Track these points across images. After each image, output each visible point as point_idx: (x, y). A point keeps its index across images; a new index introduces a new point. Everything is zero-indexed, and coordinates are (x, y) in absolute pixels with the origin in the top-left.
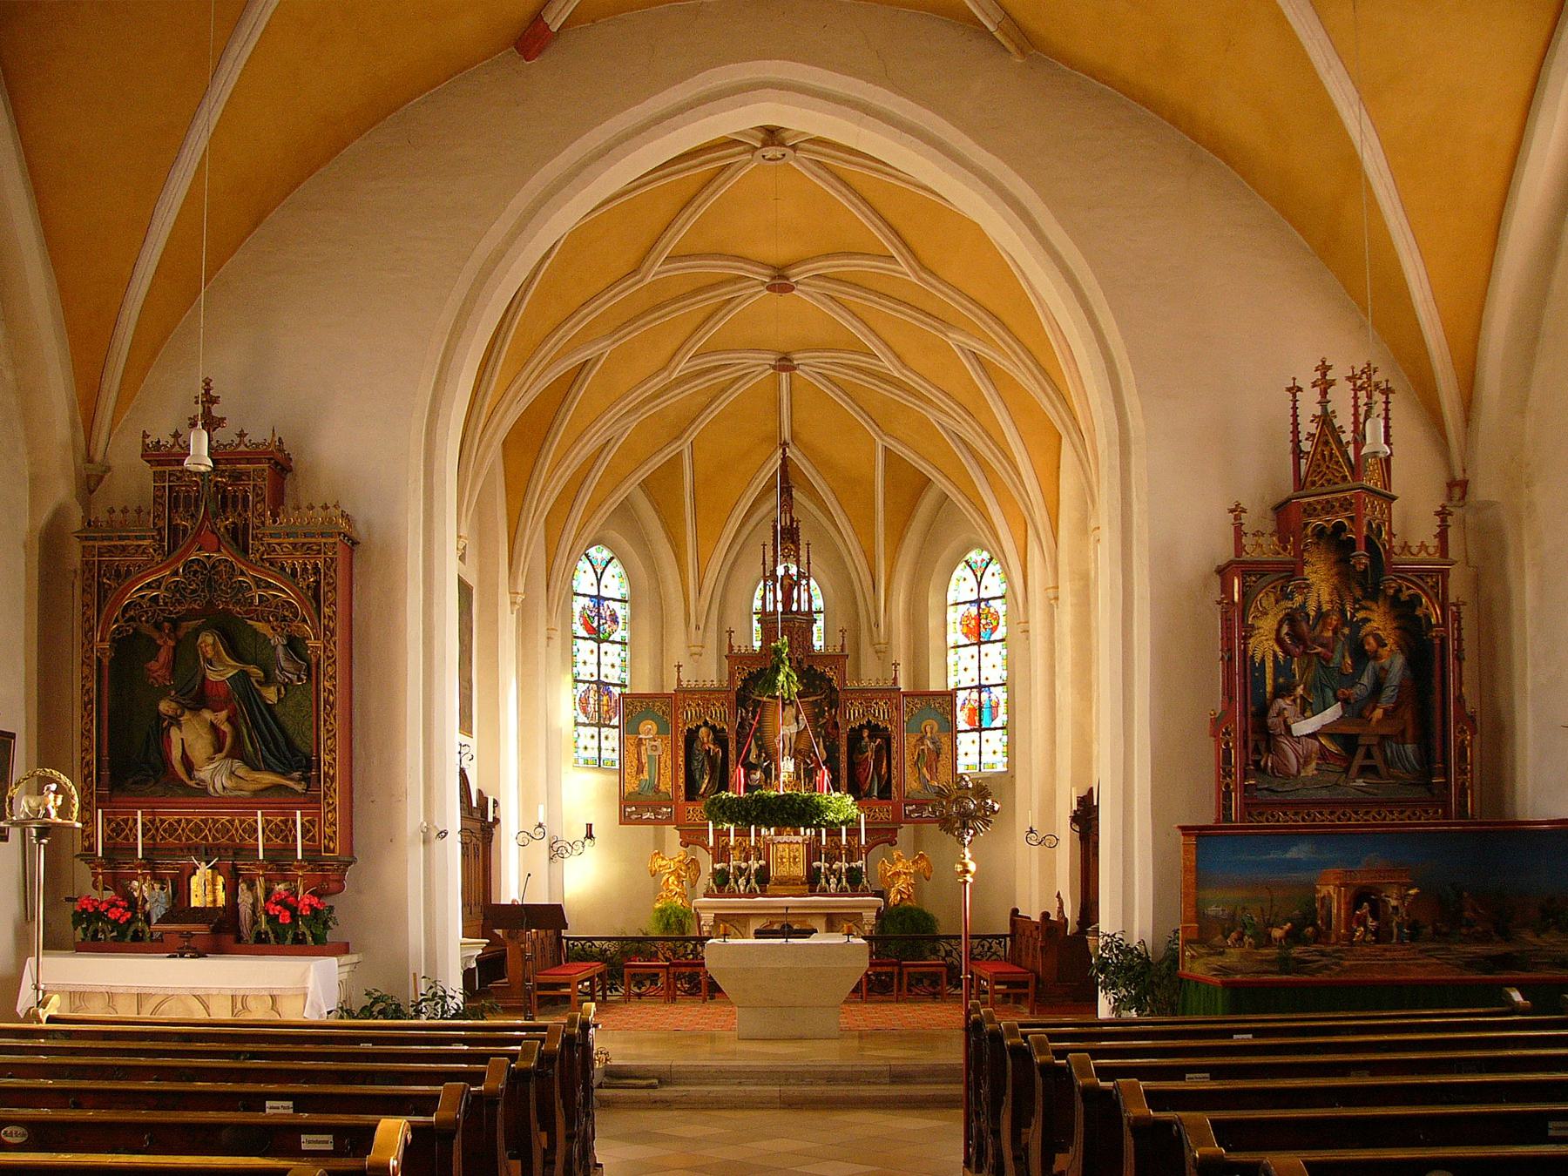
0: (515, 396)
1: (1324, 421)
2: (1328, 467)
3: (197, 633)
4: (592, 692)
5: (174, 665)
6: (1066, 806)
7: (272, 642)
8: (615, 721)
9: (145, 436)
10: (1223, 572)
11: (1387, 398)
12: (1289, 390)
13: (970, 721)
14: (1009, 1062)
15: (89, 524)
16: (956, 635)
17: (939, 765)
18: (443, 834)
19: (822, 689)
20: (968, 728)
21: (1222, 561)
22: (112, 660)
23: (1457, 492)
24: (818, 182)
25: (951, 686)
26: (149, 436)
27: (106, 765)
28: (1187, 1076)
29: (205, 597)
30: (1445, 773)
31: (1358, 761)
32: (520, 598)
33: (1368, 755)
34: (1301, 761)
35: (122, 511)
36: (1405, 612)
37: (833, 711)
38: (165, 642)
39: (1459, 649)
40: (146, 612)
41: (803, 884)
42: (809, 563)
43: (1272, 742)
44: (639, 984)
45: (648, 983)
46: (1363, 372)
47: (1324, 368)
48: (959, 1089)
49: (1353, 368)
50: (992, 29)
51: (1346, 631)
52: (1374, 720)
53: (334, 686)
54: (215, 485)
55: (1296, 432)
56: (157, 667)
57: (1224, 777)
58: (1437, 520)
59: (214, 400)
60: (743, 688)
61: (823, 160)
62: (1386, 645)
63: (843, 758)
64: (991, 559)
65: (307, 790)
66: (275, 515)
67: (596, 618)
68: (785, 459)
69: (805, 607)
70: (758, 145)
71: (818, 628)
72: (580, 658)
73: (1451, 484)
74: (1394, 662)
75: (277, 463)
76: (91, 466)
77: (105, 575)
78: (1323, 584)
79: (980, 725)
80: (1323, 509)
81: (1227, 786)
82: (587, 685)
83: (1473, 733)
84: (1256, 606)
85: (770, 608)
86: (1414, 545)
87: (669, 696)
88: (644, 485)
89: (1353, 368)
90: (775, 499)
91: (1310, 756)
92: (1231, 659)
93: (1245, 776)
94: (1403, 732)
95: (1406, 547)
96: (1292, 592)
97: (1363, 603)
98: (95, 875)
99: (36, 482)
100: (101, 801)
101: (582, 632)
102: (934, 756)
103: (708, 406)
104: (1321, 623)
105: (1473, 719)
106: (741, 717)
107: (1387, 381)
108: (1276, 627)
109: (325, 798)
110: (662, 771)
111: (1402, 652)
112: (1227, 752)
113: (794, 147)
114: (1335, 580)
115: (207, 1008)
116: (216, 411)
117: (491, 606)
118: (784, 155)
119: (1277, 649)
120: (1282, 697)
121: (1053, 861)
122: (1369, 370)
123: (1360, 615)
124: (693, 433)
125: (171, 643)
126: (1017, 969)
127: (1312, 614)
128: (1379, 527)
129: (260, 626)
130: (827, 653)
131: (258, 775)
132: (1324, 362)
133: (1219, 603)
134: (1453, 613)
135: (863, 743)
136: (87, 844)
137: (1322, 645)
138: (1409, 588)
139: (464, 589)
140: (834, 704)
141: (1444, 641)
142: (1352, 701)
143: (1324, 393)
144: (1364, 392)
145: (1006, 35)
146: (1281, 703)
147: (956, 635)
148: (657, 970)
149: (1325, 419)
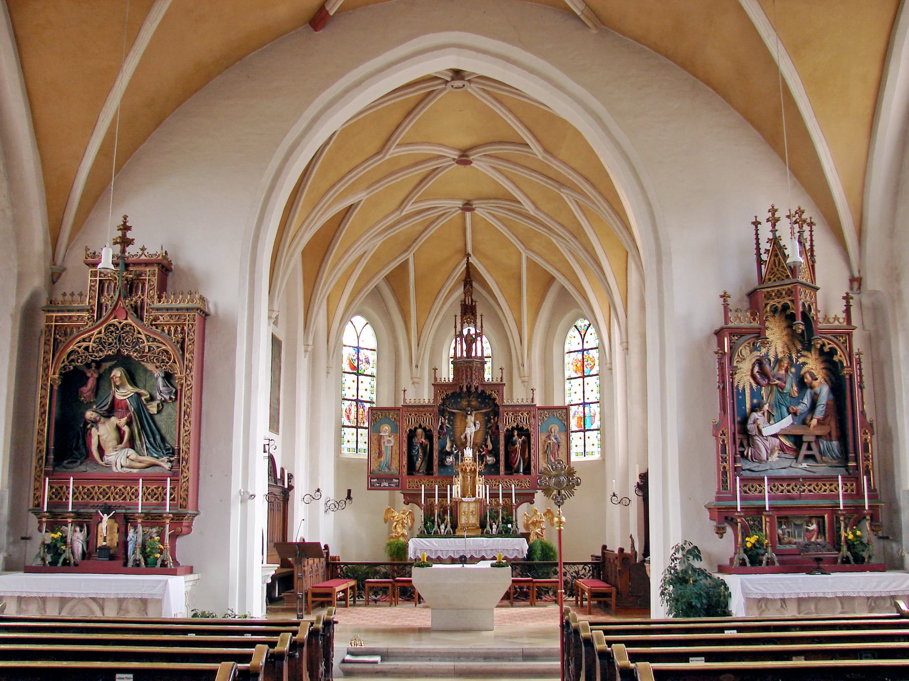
0: (310, 224)
1: (774, 244)
2: (778, 270)
3: (111, 369)
4: (353, 406)
5: (97, 390)
6: (636, 479)
7: (156, 375)
8: (366, 425)
9: (87, 249)
10: (719, 333)
11: (811, 228)
12: (753, 223)
13: (579, 425)
14: (583, 647)
15: (51, 303)
16: (570, 372)
17: (559, 452)
18: (253, 496)
19: (489, 404)
20: (577, 429)
21: (717, 327)
22: (60, 386)
23: (856, 285)
24: (484, 101)
25: (567, 403)
26: (89, 249)
27: (52, 451)
28: (690, 659)
29: (117, 347)
30: (856, 459)
31: (804, 451)
32: (310, 349)
33: (809, 448)
34: (769, 451)
35: (79, 295)
36: (827, 357)
37: (496, 418)
38: (92, 374)
39: (861, 381)
40: (81, 356)
41: (477, 528)
42: (482, 327)
43: (751, 440)
44: (376, 594)
45: (381, 593)
46: (796, 213)
47: (773, 211)
48: (557, 664)
49: (790, 210)
50: (579, 14)
51: (793, 370)
52: (812, 426)
53: (190, 402)
54: (126, 280)
55: (758, 249)
56: (87, 390)
57: (722, 462)
58: (844, 302)
59: (129, 228)
60: (443, 404)
61: (485, 88)
62: (817, 379)
63: (502, 448)
64: (590, 325)
65: (171, 468)
66: (160, 297)
67: (357, 360)
68: (468, 263)
69: (479, 354)
70: (449, 79)
71: (488, 366)
72: (346, 385)
73: (852, 280)
74: (824, 391)
75: (163, 267)
76: (54, 267)
77: (58, 334)
78: (778, 341)
79: (585, 428)
80: (776, 295)
81: (724, 467)
82: (350, 402)
83: (872, 434)
84: (738, 355)
85: (459, 355)
86: (831, 316)
87: (399, 409)
88: (387, 278)
89: (790, 210)
90: (461, 290)
91: (774, 449)
92: (724, 388)
93: (735, 461)
94: (830, 434)
95: (826, 318)
96: (759, 346)
97: (803, 353)
98: (41, 523)
99: (21, 277)
100: (47, 474)
101: (348, 369)
102: (556, 447)
103: (423, 232)
104: (777, 365)
105: (871, 425)
106: (441, 422)
107: (811, 218)
108: (751, 368)
109: (182, 473)
110: (394, 456)
111: (827, 384)
112: (724, 446)
113: (469, 81)
114: (786, 339)
115: (102, 609)
116: (129, 235)
117: (293, 354)
118: (464, 85)
119: (752, 381)
120: (756, 411)
121: (628, 515)
122: (800, 212)
123: (801, 360)
124: (415, 247)
125: (96, 376)
126: (606, 585)
127: (772, 359)
128: (809, 306)
129: (150, 366)
130: (492, 383)
131: (141, 458)
132: (773, 207)
133: (716, 353)
134: (856, 359)
135: (514, 439)
136: (36, 502)
137: (779, 379)
138: (829, 344)
139: (276, 342)
140: (496, 413)
141: (851, 376)
142: (798, 414)
143: (774, 225)
144: (797, 225)
145: (586, 17)
146: (755, 415)
147: (570, 372)
148: (386, 585)
149: (775, 241)
